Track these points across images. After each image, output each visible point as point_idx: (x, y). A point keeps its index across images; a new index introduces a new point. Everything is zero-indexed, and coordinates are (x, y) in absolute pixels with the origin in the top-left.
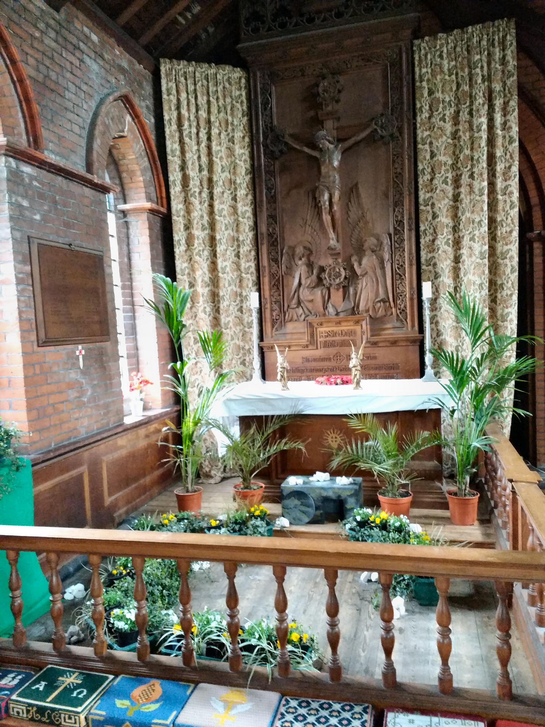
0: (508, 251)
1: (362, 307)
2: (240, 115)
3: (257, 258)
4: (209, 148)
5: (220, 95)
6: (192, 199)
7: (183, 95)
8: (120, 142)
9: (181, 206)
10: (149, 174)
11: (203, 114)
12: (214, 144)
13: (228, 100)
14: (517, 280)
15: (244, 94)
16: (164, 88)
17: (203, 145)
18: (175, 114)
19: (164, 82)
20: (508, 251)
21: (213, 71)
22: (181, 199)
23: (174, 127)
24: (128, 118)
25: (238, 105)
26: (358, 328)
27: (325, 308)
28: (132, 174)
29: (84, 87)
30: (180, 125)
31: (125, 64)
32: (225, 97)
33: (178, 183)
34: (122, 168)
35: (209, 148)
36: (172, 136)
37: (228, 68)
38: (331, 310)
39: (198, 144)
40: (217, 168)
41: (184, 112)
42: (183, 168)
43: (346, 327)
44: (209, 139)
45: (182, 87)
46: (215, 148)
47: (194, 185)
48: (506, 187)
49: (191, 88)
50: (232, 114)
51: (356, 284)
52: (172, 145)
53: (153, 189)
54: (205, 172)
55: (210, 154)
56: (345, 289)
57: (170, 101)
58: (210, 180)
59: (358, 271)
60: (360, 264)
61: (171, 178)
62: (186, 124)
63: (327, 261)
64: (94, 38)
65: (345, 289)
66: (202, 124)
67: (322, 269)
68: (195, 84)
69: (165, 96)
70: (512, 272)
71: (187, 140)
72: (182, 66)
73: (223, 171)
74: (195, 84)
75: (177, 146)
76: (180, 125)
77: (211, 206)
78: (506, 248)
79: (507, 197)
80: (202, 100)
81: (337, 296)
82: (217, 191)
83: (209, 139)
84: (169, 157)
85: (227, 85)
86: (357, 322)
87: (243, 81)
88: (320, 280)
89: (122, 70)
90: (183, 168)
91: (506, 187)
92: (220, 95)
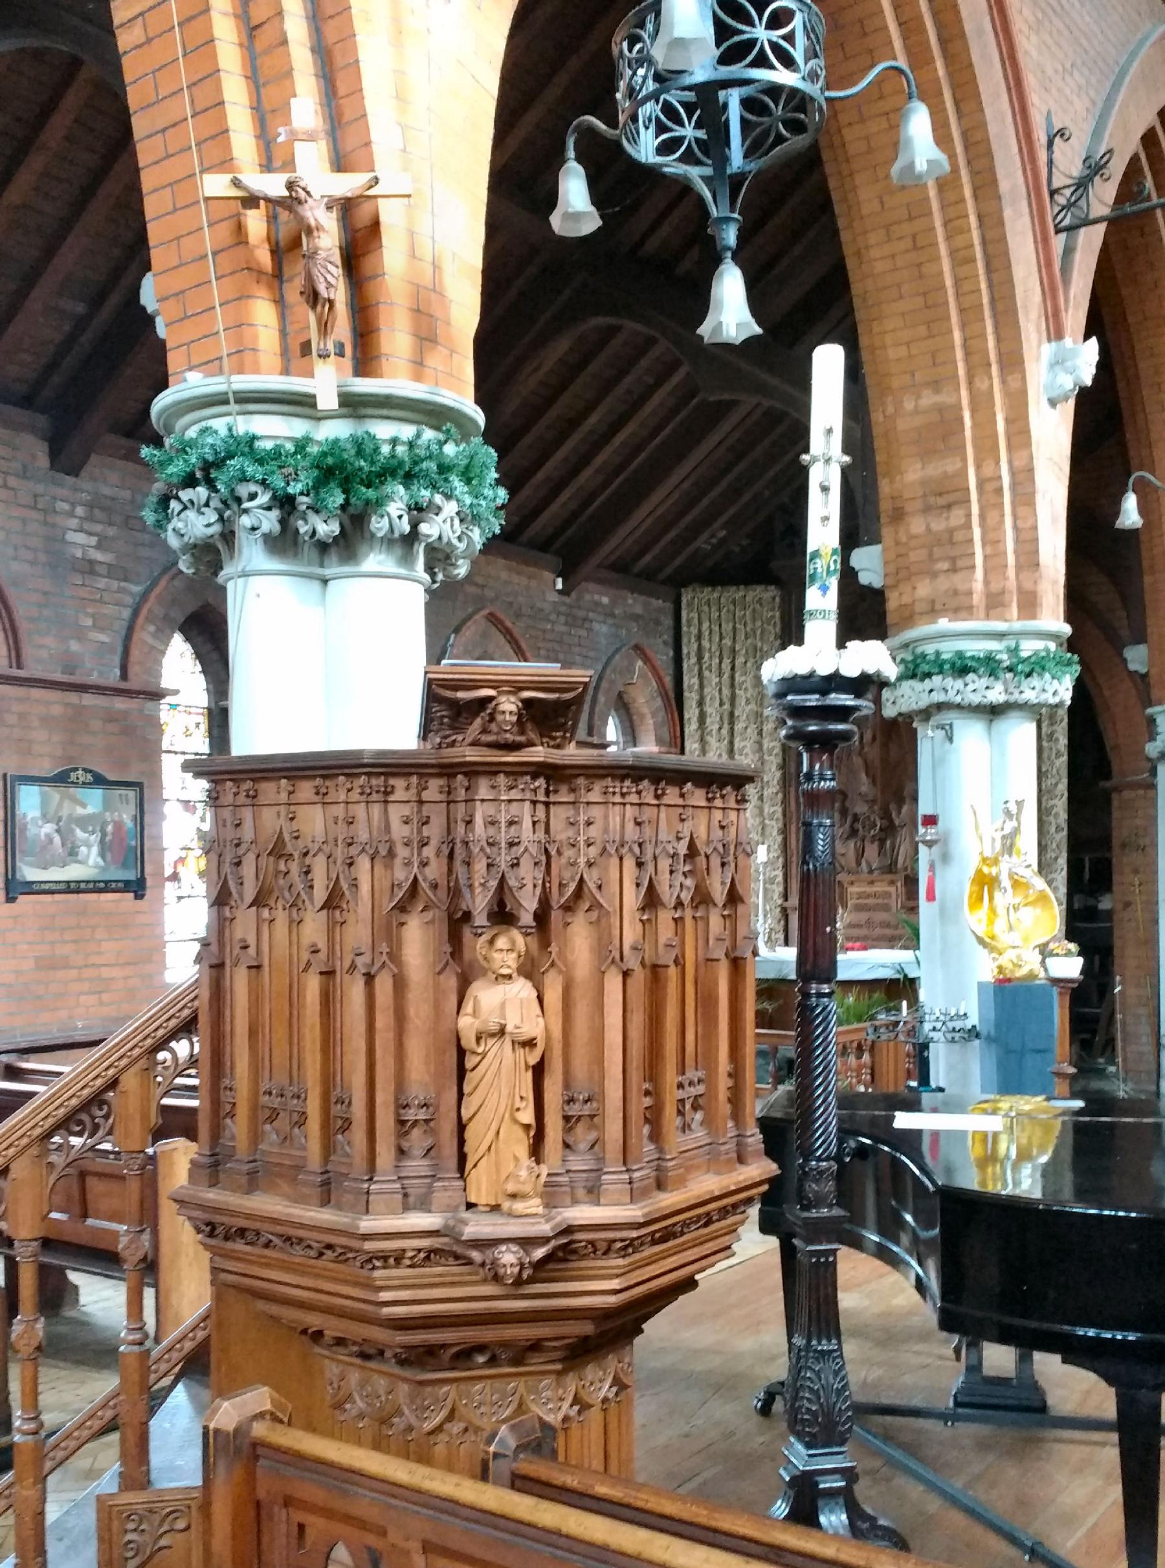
0: (1053, 807)
1: (900, 865)
2: (772, 638)
3: (785, 802)
4: (732, 678)
5: (748, 618)
6: (708, 738)
7: (706, 625)
8: (630, 689)
9: (696, 745)
10: (662, 713)
11: (727, 642)
12: (737, 675)
13: (759, 624)
14: (1065, 841)
15: (778, 614)
16: (684, 620)
17: (726, 676)
18: (695, 646)
19: (684, 614)
20: (1053, 807)
21: (741, 593)
22: (697, 737)
23: (694, 660)
24: (640, 663)
25: (771, 628)
26: (892, 889)
27: (859, 864)
28: (642, 716)
29: (592, 654)
30: (700, 657)
31: (639, 610)
32: (754, 620)
33: (695, 720)
34: (632, 711)
35: (732, 678)
36: (690, 670)
37: (759, 588)
38: (864, 864)
39: (720, 675)
40: (741, 701)
41: (706, 644)
42: (701, 703)
43: (879, 888)
44: (733, 668)
45: (704, 617)
46: (738, 678)
47: (712, 723)
48: (1052, 734)
49: (715, 615)
50: (761, 639)
51: (894, 837)
52: (690, 680)
53: (665, 729)
54: (727, 707)
55: (732, 686)
56: (882, 842)
57: (690, 633)
58: (732, 714)
59: (897, 823)
60: (899, 812)
61: (686, 716)
62: (707, 656)
63: (861, 808)
64: (605, 600)
65: (882, 842)
66: (725, 654)
67: (856, 818)
68: (720, 610)
69: (685, 629)
70: (1058, 829)
71: (706, 673)
72: (707, 593)
73: (748, 702)
74: (720, 610)
75: (695, 680)
76: (700, 657)
77: (731, 743)
78: (1051, 803)
79: (1052, 744)
80: (727, 627)
81: (872, 851)
82: (739, 726)
83: (733, 668)
84: (686, 694)
85: (758, 606)
86: (892, 883)
87: (778, 600)
88: (853, 833)
89: (636, 618)
90: (701, 703)
91: (1052, 734)
92: (748, 618)
